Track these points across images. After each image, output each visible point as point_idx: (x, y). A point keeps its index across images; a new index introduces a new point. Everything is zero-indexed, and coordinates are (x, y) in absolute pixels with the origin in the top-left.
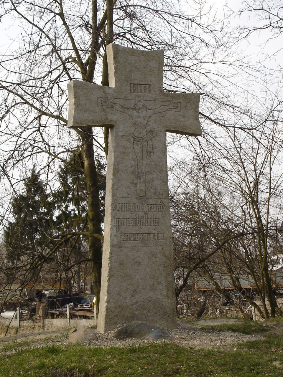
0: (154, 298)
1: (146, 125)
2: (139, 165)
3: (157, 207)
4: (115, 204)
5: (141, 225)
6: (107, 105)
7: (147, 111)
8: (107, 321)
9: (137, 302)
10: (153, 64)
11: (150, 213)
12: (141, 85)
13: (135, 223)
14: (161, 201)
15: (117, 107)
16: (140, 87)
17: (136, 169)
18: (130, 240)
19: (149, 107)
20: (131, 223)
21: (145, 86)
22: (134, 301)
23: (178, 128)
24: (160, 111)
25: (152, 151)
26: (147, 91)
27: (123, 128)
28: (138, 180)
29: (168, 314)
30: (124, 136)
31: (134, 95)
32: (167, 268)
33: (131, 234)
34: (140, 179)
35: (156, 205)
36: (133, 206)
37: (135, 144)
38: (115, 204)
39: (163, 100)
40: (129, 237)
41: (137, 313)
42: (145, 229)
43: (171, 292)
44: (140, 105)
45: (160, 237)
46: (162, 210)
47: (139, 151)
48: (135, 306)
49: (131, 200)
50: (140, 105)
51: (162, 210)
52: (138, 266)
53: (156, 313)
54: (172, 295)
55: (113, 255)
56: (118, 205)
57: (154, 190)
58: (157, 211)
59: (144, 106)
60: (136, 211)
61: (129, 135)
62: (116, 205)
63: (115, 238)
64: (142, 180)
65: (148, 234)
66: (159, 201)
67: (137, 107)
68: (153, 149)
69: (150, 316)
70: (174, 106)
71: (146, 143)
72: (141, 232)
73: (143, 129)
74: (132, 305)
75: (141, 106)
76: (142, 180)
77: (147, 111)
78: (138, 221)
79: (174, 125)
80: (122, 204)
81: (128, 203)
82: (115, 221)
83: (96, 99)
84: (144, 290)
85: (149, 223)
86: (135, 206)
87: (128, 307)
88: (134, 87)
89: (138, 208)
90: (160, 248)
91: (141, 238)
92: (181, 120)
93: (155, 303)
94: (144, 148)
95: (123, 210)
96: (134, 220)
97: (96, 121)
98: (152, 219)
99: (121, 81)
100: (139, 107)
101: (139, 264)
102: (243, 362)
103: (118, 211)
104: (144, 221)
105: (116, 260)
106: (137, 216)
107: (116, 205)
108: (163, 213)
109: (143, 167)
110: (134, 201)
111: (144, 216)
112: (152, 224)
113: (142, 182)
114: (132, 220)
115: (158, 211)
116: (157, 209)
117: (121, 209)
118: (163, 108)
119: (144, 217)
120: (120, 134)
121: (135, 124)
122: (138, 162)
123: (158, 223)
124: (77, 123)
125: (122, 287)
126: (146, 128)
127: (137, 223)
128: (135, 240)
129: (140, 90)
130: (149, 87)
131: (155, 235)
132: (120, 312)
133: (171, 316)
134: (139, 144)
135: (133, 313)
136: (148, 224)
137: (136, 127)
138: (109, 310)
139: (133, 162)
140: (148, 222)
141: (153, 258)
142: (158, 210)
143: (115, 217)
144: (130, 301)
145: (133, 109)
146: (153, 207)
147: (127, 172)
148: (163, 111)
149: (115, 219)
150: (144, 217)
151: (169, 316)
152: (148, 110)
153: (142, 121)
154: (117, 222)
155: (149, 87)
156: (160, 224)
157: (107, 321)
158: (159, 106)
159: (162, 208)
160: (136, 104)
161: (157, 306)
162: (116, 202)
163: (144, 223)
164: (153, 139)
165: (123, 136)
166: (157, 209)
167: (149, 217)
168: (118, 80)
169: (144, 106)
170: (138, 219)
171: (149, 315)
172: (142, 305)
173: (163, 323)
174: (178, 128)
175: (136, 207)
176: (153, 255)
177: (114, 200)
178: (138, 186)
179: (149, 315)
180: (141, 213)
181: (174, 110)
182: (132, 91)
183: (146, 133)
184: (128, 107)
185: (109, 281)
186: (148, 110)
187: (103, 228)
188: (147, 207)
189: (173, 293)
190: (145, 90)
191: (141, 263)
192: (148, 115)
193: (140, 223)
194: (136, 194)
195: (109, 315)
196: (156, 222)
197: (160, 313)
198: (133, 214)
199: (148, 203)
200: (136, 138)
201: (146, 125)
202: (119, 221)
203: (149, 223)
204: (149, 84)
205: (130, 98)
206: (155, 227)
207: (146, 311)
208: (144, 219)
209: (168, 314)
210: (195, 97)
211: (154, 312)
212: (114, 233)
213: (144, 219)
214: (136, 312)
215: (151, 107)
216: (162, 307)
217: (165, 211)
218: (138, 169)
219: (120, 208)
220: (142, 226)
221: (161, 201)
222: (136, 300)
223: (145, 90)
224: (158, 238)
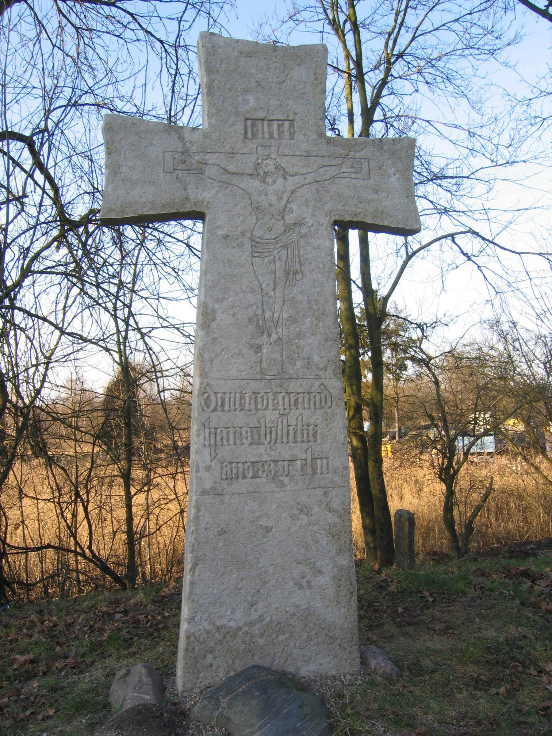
0: (303, 607)
1: (284, 210)
2: (267, 303)
3: (312, 398)
4: (206, 396)
5: (273, 442)
6: (188, 168)
7: (285, 179)
8: (187, 663)
9: (261, 618)
10: (300, 74)
11: (294, 414)
12: (271, 123)
13: (256, 437)
14: (322, 384)
15: (211, 171)
16: (269, 126)
17: (259, 312)
18: (244, 477)
19: (290, 170)
20: (247, 438)
21: (280, 123)
22: (255, 616)
23: (362, 215)
24: (319, 179)
25: (299, 268)
26: (287, 134)
27: (226, 219)
28: (265, 338)
29: (339, 641)
30: (227, 236)
31: (252, 145)
32: (337, 537)
33: (246, 462)
34: (269, 336)
35: (308, 393)
36: (250, 399)
37: (257, 254)
38: (206, 396)
39: (325, 154)
40: (241, 469)
41: (262, 641)
42: (284, 451)
43: (344, 592)
44: (270, 165)
45: (319, 467)
46: (323, 404)
47: (265, 271)
48: (258, 626)
49: (247, 384)
50: (270, 165)
51: (323, 404)
52: (264, 536)
53: (309, 639)
54: (348, 597)
55: (201, 514)
56: (212, 397)
57: (304, 359)
58: (312, 406)
59: (278, 167)
60: (260, 410)
61: (243, 233)
62: (209, 396)
63: (207, 474)
64: (274, 336)
65: (288, 461)
66: (317, 384)
67: (261, 172)
68: (301, 265)
69: (295, 647)
70: (352, 167)
71: (284, 252)
72: (272, 458)
73: (276, 220)
74: (251, 624)
75: (271, 168)
76: (274, 336)
77: (285, 179)
78: (263, 433)
79: (354, 209)
80: (224, 393)
81: (239, 391)
82: (207, 435)
83: (160, 156)
84: (279, 591)
85: (291, 437)
86: (256, 397)
87: (240, 628)
88: (253, 125)
89: (265, 401)
90: (319, 492)
91: (273, 472)
92: (371, 197)
93: (307, 619)
94: (278, 263)
95: (226, 407)
96: (255, 430)
97: (160, 205)
98: (299, 427)
99: (222, 113)
100: (266, 171)
101: (268, 531)
102: (106, 266)
103: (215, 410)
104: (279, 432)
105: (208, 526)
106: (262, 421)
107: (209, 396)
108: (325, 412)
109: (277, 307)
110: (254, 385)
111: (280, 420)
112: (299, 439)
113: (275, 342)
114: (249, 430)
115: (315, 408)
116: (312, 403)
117: (223, 405)
118: (326, 171)
119: (280, 423)
120: (220, 232)
121: (257, 208)
122: (263, 296)
123: (315, 435)
124: (111, 210)
125: (225, 587)
126: (283, 217)
127: (263, 438)
128: (254, 477)
129: (269, 132)
130: (292, 126)
131: (306, 464)
132: (219, 641)
133: (345, 645)
134: (265, 254)
135: (254, 643)
136: (288, 438)
137: (260, 216)
138: (192, 639)
139: (251, 297)
140: (321, 401)
141: (302, 516)
142: (315, 405)
143: (207, 426)
144: (244, 617)
145: (251, 175)
146: (300, 400)
147: (237, 319)
148: (324, 178)
149: (207, 430)
150: (280, 423)
151: (340, 646)
152: (288, 177)
153: (275, 202)
154: (212, 436)
155: (292, 126)
156: (319, 437)
157: (187, 663)
158: (316, 168)
159: (323, 399)
160: (258, 164)
161: (312, 625)
162: (208, 389)
163: (279, 436)
164: (302, 242)
165: (226, 237)
166: (312, 403)
167: (292, 421)
168: (213, 111)
169: (278, 167)
170: (263, 430)
171: (292, 644)
172: (275, 623)
173: (326, 660)
174: (362, 215)
175: (260, 400)
176: (301, 511)
177: (204, 386)
178: (265, 350)
179: (292, 644)
180: (271, 415)
181: (353, 176)
182: (249, 135)
183: (283, 229)
184: (240, 172)
185: (194, 572)
186: (288, 177)
187: (350, 458)
188: (287, 400)
189: (351, 593)
190: (281, 133)
191: (271, 528)
192: (290, 188)
193: (268, 436)
194: (259, 370)
195: (194, 648)
196: (308, 434)
197: (320, 639)
198: (252, 417)
199: (289, 391)
200: (258, 240)
201: (284, 210)
202: (216, 434)
203: (291, 437)
204: (291, 118)
205: (245, 150)
206: (305, 446)
207: (285, 637)
208: (280, 427)
209: (339, 641)
210: (402, 148)
211: (304, 637)
212: (204, 462)
213: (280, 427)
214: (258, 640)
215: (296, 169)
216: (322, 626)
217: (330, 407)
218: (263, 311)
219: (220, 403)
220: (276, 442)
221: (322, 384)
222: (259, 612)
223: (281, 133)
224: (314, 472)
